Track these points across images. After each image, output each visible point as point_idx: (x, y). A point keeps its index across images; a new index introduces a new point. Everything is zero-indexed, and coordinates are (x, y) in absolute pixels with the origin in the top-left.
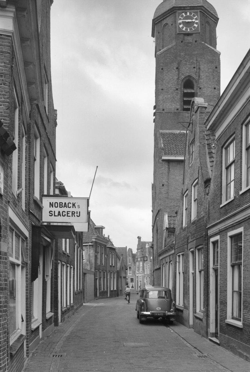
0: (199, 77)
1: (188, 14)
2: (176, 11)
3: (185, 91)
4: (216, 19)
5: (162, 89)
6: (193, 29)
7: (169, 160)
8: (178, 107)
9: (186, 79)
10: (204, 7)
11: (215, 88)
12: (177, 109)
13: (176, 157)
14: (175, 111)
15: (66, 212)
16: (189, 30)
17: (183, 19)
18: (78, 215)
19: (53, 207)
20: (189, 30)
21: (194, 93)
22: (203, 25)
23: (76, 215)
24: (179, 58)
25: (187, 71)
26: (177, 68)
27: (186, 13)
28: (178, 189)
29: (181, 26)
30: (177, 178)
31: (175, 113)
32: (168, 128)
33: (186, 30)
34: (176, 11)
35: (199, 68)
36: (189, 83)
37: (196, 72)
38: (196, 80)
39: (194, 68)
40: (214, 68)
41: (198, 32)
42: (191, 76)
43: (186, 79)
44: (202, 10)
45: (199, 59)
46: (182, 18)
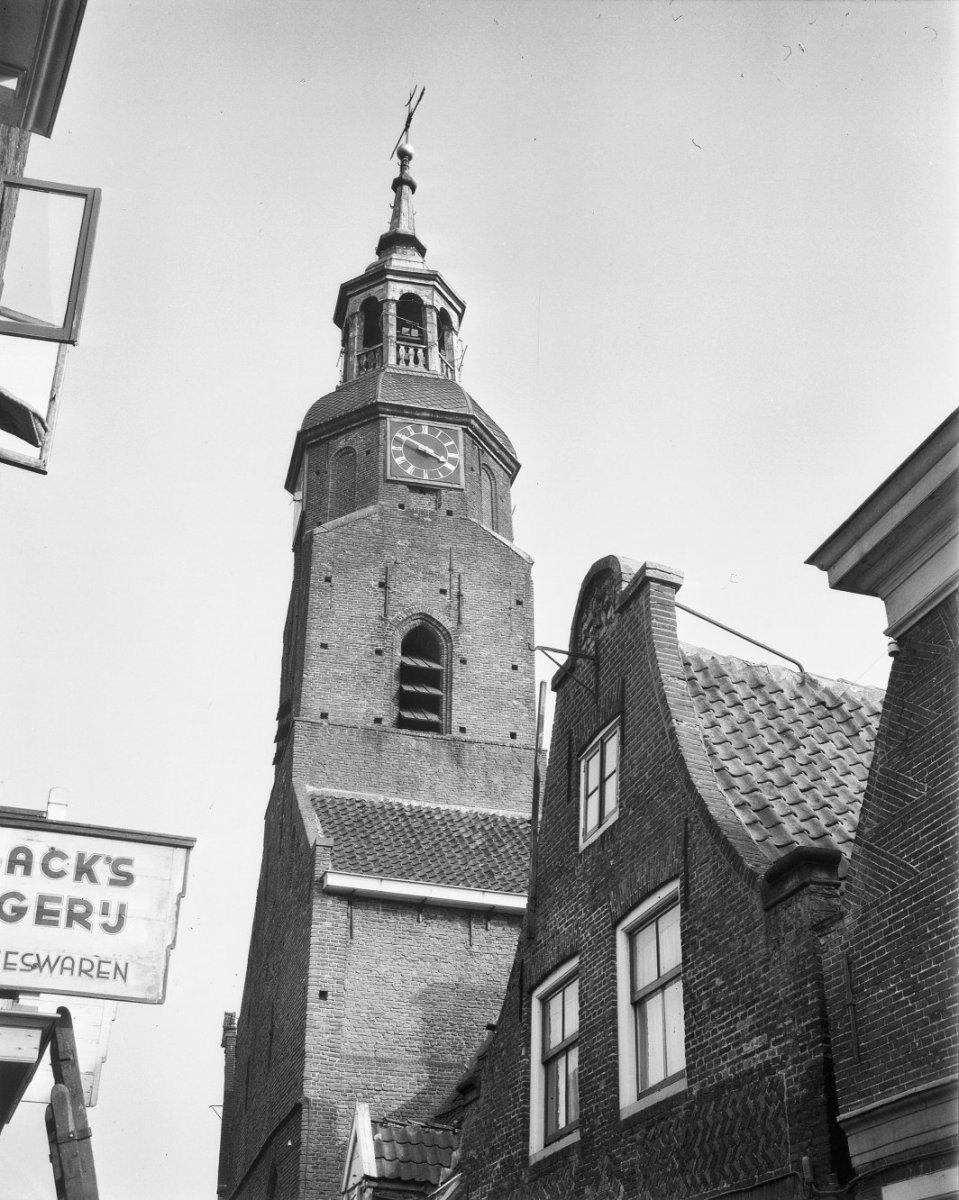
0: (459, 623)
1: (425, 431)
2: (384, 415)
3: (409, 662)
4: (513, 465)
5: (324, 646)
6: (442, 476)
7: (354, 890)
8: (379, 712)
9: (412, 623)
10: (477, 420)
11: (515, 668)
12: (378, 721)
13: (384, 882)
14: (369, 725)
15: (65, 902)
16: (426, 476)
17: (414, 437)
18: (112, 921)
19: (27, 871)
20: (426, 476)
21: (438, 673)
22: (472, 470)
23: (95, 919)
24: (389, 556)
25: (418, 597)
26: (381, 585)
27: (418, 428)
28: (387, 1015)
29: (399, 461)
30: (383, 969)
31: (367, 729)
32: (338, 780)
33: (416, 472)
34: (384, 415)
35: (459, 596)
36: (424, 640)
37: (450, 606)
38: (448, 633)
39: (443, 592)
40: (514, 603)
41: (457, 486)
42: (430, 617)
43: (412, 623)
44: (471, 426)
45: (459, 568)
46: (412, 433)
